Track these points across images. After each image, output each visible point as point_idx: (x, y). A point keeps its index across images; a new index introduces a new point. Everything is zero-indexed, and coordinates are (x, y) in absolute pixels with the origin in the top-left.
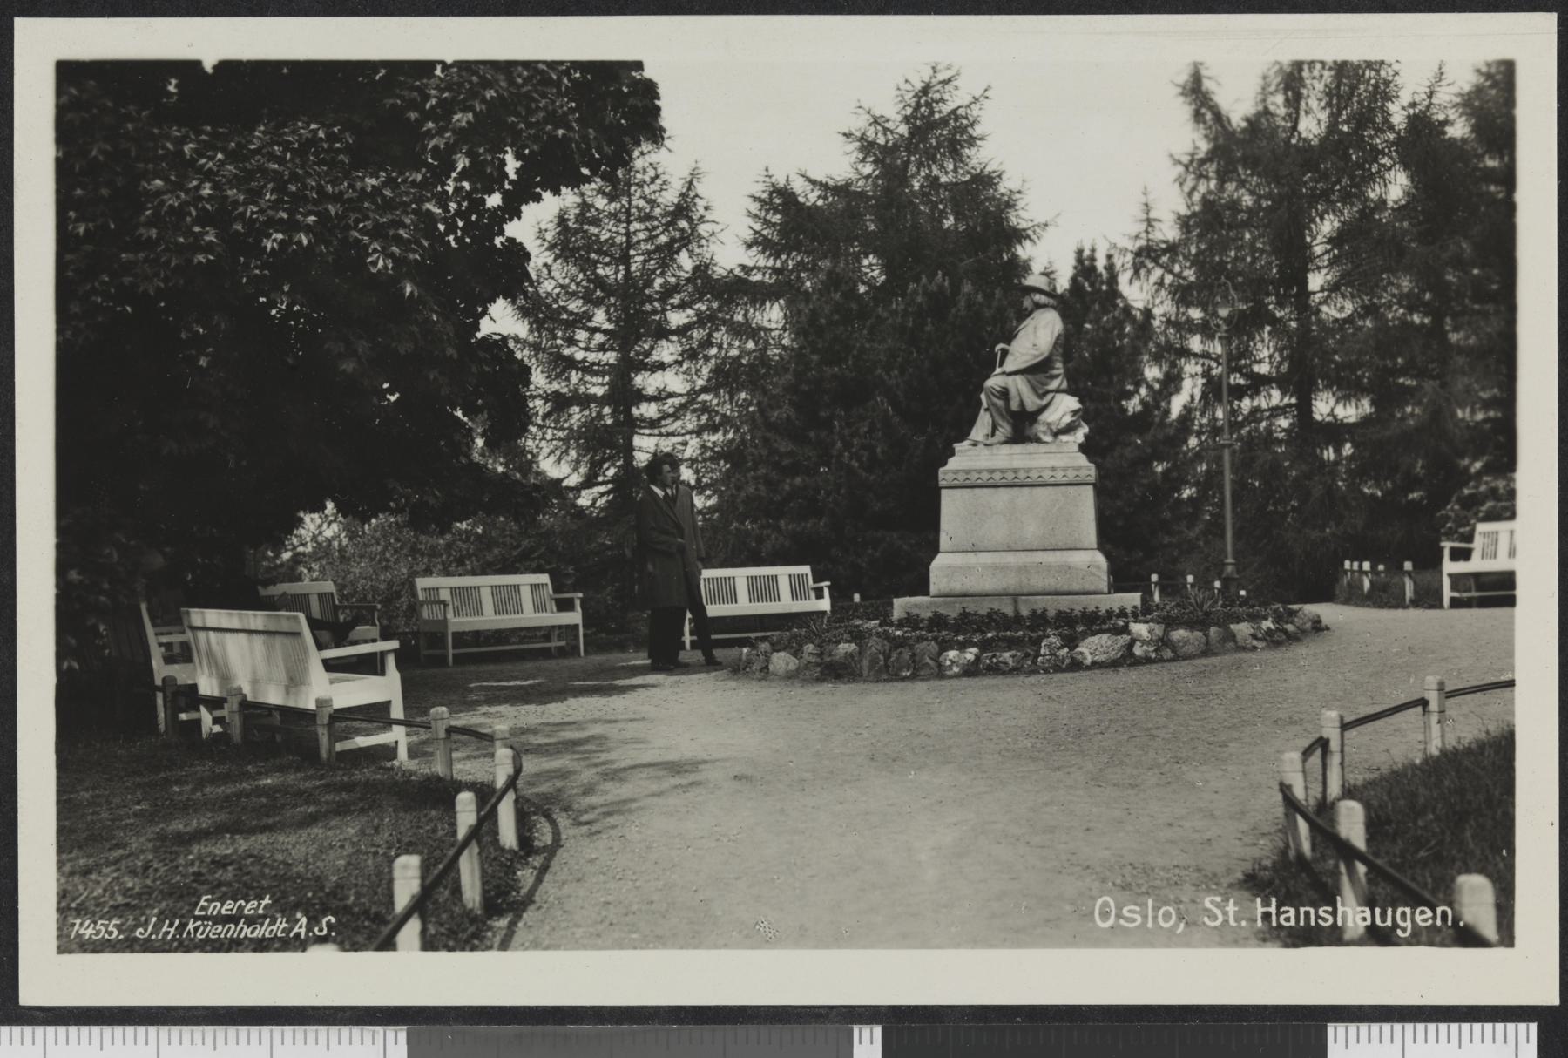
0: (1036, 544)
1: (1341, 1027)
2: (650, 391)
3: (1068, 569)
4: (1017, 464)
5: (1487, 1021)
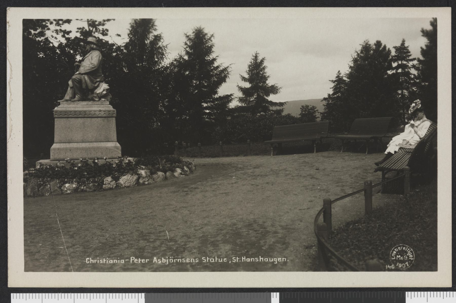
1: (409, 293)
2: (64, 39)
5: (57, 293)
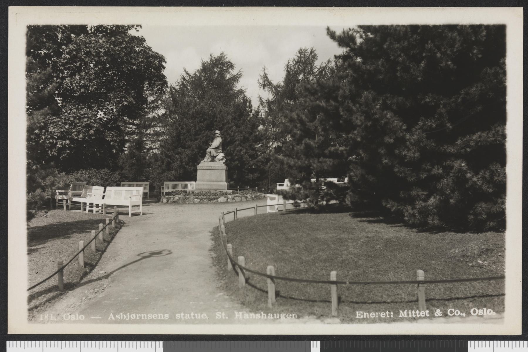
4: (212, 165)
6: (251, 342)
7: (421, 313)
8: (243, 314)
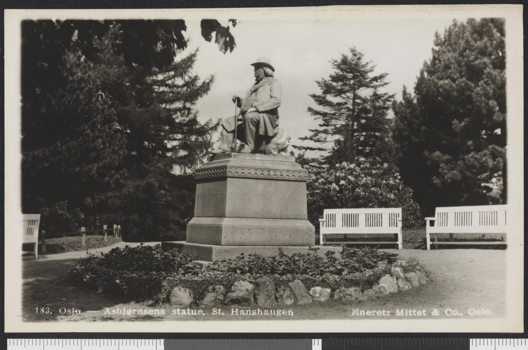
0: (278, 215)
3: (296, 230)
4: (259, 165)
6: (252, 340)
7: (418, 313)
8: (404, 311)
